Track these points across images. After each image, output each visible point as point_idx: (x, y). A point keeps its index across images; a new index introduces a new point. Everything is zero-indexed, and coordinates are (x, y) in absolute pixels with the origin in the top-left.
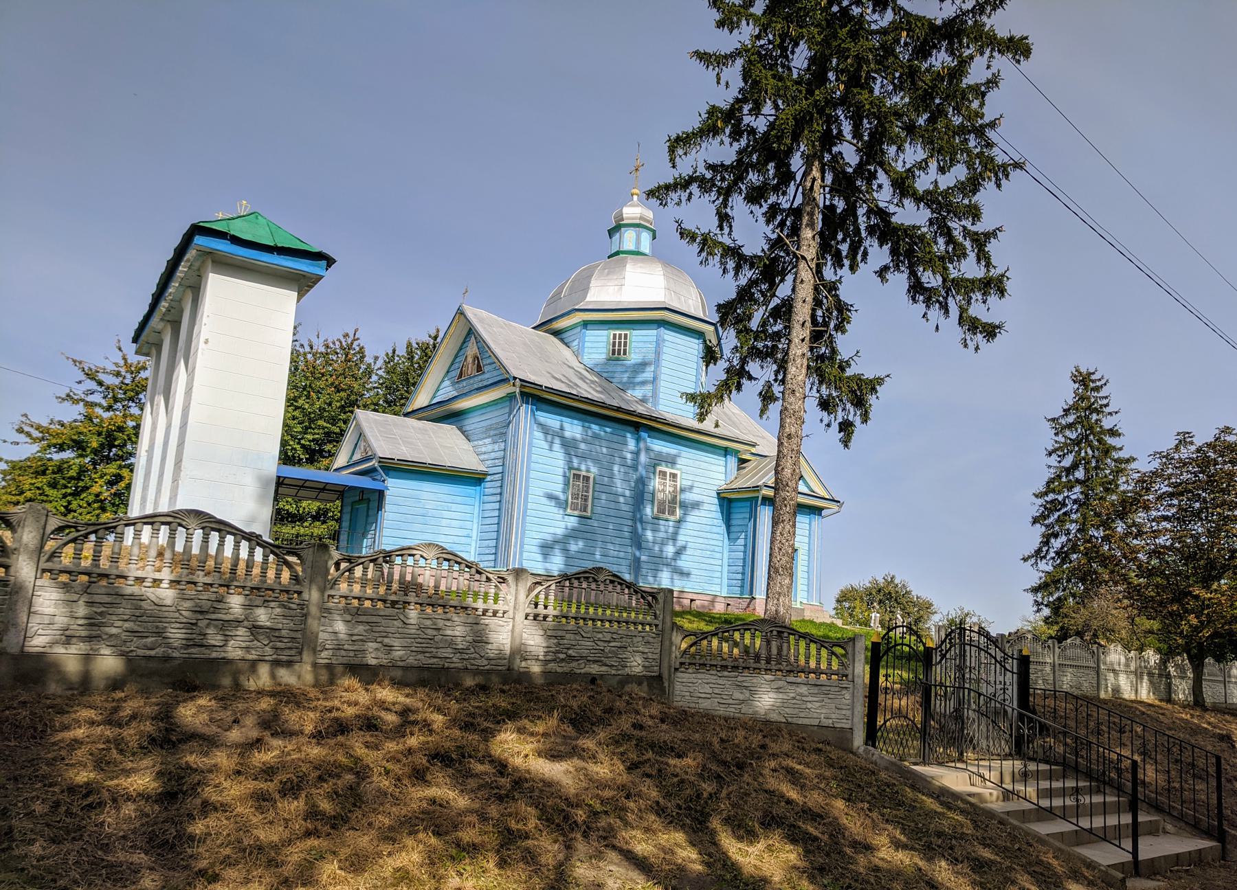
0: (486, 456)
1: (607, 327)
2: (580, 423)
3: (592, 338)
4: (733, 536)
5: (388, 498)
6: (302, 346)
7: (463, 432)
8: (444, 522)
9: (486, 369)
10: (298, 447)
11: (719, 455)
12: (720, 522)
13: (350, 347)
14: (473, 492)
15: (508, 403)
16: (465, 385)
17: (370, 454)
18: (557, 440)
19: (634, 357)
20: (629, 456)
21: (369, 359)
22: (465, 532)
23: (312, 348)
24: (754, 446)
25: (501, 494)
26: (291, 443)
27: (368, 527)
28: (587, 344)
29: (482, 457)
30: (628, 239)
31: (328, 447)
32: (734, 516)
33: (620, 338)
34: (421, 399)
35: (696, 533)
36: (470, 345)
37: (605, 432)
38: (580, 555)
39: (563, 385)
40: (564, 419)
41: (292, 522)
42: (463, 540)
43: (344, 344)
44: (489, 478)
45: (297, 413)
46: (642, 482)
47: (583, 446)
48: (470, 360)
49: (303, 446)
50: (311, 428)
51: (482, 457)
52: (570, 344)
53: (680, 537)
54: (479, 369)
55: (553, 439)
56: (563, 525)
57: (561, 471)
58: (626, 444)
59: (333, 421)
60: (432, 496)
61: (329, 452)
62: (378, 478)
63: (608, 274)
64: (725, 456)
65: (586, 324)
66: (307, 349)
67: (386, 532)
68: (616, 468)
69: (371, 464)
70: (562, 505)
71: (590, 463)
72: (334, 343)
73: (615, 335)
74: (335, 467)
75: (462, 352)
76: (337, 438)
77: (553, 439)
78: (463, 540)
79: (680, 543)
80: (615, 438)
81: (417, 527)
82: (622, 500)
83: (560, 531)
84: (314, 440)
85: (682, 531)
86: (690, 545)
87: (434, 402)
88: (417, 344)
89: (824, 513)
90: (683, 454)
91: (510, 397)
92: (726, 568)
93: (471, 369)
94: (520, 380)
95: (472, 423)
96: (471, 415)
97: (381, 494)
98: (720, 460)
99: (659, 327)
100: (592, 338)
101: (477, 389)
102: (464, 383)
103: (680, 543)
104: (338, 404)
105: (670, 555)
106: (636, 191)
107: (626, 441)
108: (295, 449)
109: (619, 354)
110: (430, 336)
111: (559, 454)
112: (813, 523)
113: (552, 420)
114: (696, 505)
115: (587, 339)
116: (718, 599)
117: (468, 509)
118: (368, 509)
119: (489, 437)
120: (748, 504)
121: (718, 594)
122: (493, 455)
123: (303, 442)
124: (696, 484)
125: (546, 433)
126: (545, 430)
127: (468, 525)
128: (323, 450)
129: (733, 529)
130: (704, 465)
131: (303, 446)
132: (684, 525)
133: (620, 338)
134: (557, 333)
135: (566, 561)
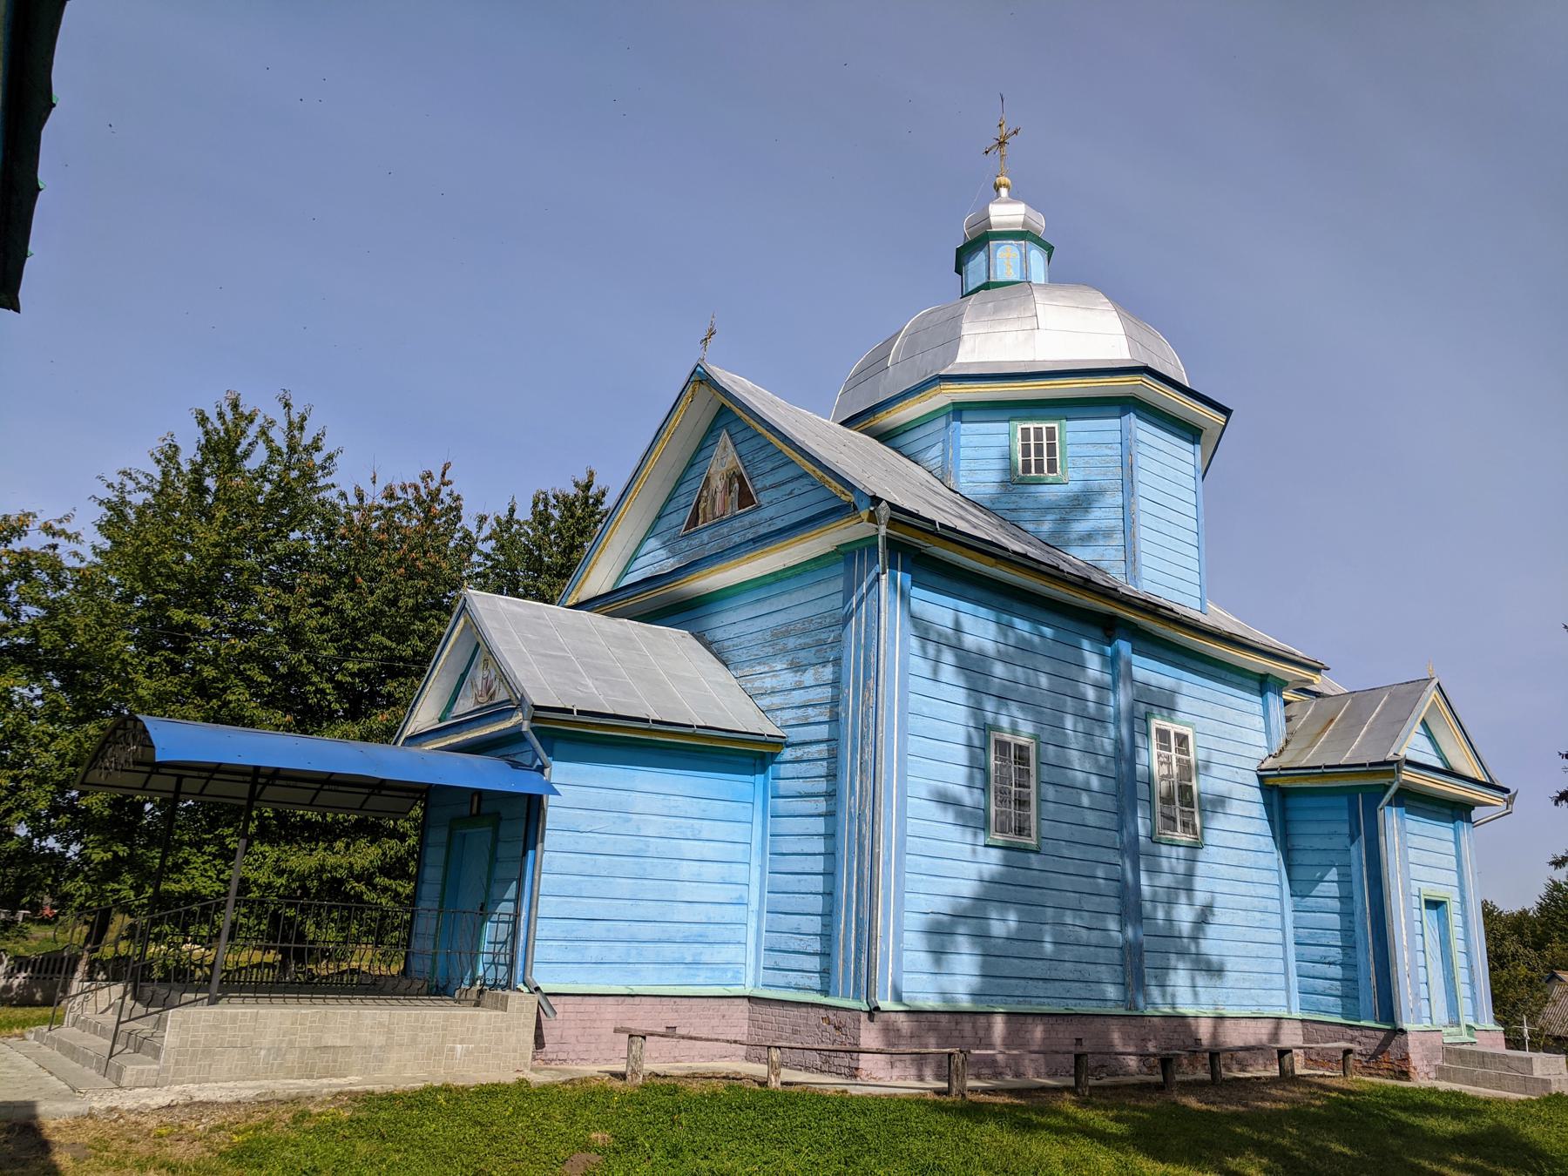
0: (777, 700)
1: (1008, 414)
2: (991, 615)
3: (976, 440)
4: (1300, 873)
5: (555, 812)
6: (343, 495)
7: (708, 645)
8: (687, 869)
9: (763, 498)
10: (328, 687)
11: (1251, 691)
12: (1268, 843)
13: (434, 496)
14: (749, 787)
15: (840, 569)
16: (705, 541)
17: (502, 695)
18: (948, 657)
19: (1070, 478)
20: (1091, 693)
21: (468, 522)
22: (732, 893)
23: (361, 499)
24: (1317, 670)
25: (830, 795)
26: (315, 679)
27: (496, 890)
28: (964, 453)
29: (766, 702)
30: (1005, 260)
31: (390, 686)
32: (1296, 828)
33: (1038, 437)
34: (599, 578)
35: (1233, 873)
36: (718, 451)
37: (1042, 636)
38: (1017, 948)
39: (966, 525)
40: (964, 605)
41: (308, 840)
42: (731, 913)
43: (423, 492)
44: (788, 754)
45: (328, 620)
46: (1125, 756)
47: (999, 669)
48: (718, 483)
49: (339, 686)
50: (356, 649)
51: (766, 702)
52: (920, 457)
53: (1199, 883)
54: (745, 498)
55: (939, 651)
56: (972, 870)
57: (960, 734)
58: (1082, 666)
59: (401, 635)
60: (657, 804)
61: (390, 695)
62: (526, 759)
63: (996, 311)
64: (1262, 693)
65: (959, 411)
66: (353, 501)
67: (546, 906)
68: (1069, 722)
69: (508, 724)
70: (974, 820)
71: (1014, 709)
72: (404, 489)
73: (1025, 431)
74: (407, 733)
75: (696, 470)
76: (418, 667)
77: (939, 651)
78: (731, 913)
79: (1200, 898)
80: (1061, 651)
81: (624, 887)
82: (1085, 800)
83: (968, 888)
84: (360, 673)
85: (1200, 868)
86: (1220, 900)
87: (624, 583)
88: (555, 497)
89: (1476, 814)
90: (1185, 687)
91: (849, 555)
92: (1291, 948)
93: (721, 500)
94: (893, 507)
95: (730, 624)
96: (727, 604)
97: (532, 808)
98: (1252, 703)
99: (1124, 412)
100: (976, 440)
101: (754, 541)
102: (705, 536)
103: (1200, 898)
104: (411, 602)
105: (1185, 928)
106: (1003, 179)
107: (1082, 658)
108: (323, 692)
109: (1039, 469)
110: (577, 485)
111: (952, 692)
112: (1464, 839)
113: (938, 609)
114: (1219, 802)
115: (963, 440)
116: (1285, 1025)
117: (738, 832)
118: (496, 840)
119: (785, 651)
120: (1344, 801)
121: (1283, 1013)
122: (798, 697)
123: (339, 677)
124: (1216, 757)
125: (924, 638)
126: (922, 629)
127: (739, 872)
128: (379, 694)
129: (1298, 858)
130: (1231, 715)
131: (339, 686)
132: (1202, 855)
133: (1038, 437)
134: (886, 437)
135: (983, 966)
